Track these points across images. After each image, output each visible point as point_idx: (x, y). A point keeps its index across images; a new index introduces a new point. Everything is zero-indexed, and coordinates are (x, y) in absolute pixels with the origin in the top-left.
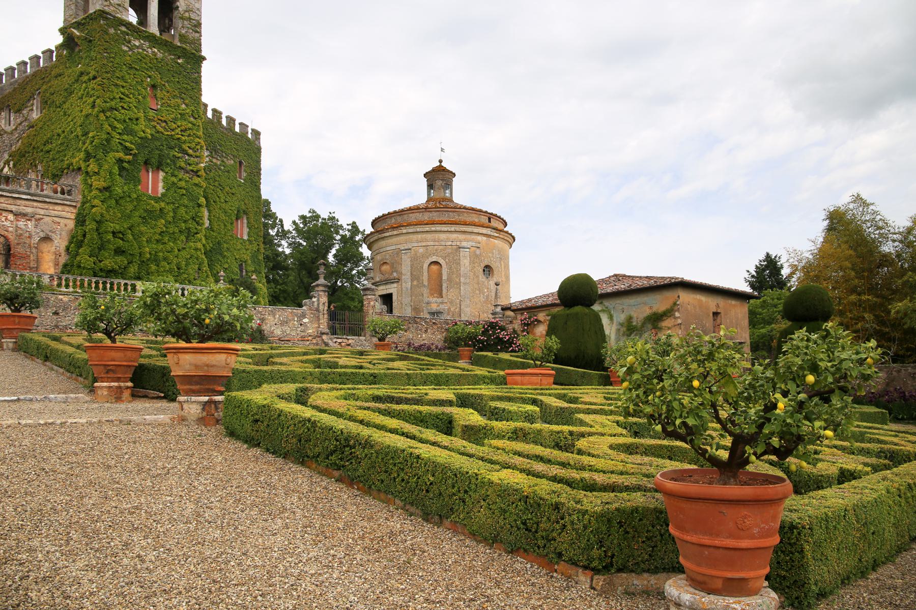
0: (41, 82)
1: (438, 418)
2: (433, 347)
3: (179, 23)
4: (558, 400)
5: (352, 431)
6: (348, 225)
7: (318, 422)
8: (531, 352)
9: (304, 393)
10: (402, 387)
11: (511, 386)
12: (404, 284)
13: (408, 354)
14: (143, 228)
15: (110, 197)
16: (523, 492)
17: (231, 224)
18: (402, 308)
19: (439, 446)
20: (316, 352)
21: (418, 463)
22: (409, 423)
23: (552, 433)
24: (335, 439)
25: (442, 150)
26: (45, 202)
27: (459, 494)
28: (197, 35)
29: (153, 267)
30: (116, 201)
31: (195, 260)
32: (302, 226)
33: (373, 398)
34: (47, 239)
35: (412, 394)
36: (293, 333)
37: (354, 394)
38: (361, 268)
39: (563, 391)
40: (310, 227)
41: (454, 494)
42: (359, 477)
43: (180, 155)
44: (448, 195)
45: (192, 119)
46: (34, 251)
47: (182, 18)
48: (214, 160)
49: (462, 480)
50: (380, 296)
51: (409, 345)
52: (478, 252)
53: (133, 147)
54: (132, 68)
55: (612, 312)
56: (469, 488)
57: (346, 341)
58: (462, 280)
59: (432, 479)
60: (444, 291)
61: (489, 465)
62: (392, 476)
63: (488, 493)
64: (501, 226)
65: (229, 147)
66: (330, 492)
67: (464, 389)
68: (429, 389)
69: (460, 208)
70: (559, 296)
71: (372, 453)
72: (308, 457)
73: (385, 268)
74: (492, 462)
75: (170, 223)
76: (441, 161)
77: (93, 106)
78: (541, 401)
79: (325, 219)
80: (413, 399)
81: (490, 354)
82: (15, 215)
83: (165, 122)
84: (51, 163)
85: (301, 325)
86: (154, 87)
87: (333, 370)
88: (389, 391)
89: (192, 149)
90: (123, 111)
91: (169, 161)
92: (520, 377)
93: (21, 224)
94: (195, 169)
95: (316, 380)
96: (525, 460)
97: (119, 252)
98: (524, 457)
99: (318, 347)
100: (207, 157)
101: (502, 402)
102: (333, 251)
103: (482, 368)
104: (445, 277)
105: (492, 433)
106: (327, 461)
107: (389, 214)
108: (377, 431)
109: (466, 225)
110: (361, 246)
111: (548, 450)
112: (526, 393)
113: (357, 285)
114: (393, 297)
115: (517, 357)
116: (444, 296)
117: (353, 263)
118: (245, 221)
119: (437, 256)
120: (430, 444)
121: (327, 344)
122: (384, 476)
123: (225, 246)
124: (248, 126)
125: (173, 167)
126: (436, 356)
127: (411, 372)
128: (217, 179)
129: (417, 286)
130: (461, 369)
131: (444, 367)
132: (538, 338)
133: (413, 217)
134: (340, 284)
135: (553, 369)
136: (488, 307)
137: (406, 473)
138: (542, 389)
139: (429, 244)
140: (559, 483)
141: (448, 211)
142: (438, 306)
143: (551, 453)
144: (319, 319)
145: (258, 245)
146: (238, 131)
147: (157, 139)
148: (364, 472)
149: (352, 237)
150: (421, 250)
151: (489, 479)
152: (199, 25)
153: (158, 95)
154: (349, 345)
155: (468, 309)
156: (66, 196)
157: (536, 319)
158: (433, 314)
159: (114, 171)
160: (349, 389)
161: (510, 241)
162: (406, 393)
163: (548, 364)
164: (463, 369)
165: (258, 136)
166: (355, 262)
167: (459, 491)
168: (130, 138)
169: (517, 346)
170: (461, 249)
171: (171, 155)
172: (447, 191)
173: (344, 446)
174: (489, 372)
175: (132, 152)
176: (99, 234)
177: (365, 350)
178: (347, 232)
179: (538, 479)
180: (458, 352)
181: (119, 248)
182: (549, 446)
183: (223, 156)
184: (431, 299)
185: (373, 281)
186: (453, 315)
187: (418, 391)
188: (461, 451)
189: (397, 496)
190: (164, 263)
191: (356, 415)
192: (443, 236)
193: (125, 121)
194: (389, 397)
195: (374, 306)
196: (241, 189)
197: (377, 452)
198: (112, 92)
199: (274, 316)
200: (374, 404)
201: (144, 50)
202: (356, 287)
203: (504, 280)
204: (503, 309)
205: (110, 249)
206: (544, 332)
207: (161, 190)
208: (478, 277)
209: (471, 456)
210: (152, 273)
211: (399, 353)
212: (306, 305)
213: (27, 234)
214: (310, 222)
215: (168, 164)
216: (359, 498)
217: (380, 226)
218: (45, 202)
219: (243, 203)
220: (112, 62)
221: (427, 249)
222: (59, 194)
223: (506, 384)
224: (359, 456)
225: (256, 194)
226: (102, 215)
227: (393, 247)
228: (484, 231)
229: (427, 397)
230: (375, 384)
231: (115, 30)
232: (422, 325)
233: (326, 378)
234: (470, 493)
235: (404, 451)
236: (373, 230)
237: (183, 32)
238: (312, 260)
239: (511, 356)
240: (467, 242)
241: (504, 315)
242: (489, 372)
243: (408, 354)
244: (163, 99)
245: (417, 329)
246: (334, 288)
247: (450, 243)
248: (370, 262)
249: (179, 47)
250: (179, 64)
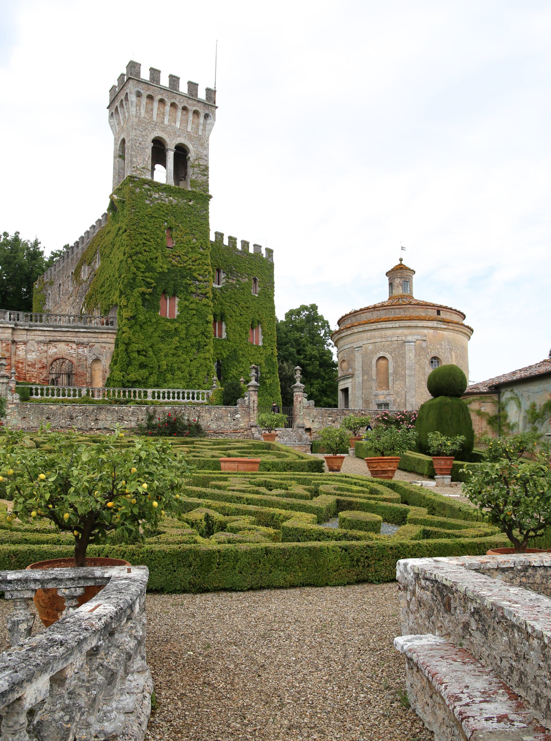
0: (100, 239)
3: (190, 171)
12: (357, 379)
14: (161, 346)
15: (135, 324)
17: (246, 333)
26: (95, 332)
28: (206, 177)
29: (169, 376)
30: (141, 326)
31: (205, 368)
34: (97, 360)
36: (227, 427)
43: (191, 282)
45: (201, 250)
46: (89, 370)
47: (193, 167)
48: (230, 281)
52: (424, 344)
53: (152, 281)
54: (152, 217)
55: (520, 399)
58: (407, 372)
60: (391, 384)
65: (243, 267)
75: (183, 339)
76: (401, 260)
77: (125, 254)
82: (77, 344)
83: (179, 256)
84: (104, 302)
85: (234, 420)
86: (170, 229)
89: (202, 275)
90: (145, 254)
91: (182, 288)
93: (80, 351)
94: (204, 292)
97: (142, 366)
100: (223, 279)
104: (391, 371)
116: (390, 388)
118: (260, 330)
119: (384, 351)
123: (241, 352)
124: (261, 247)
125: (185, 293)
128: (233, 296)
133: (364, 317)
139: (377, 340)
141: (394, 309)
142: (385, 397)
144: (249, 414)
145: (272, 349)
146: (253, 252)
147: (173, 272)
150: (371, 347)
152: (207, 168)
153: (174, 236)
155: (413, 399)
156: (110, 326)
158: (379, 405)
159: (139, 303)
165: (270, 254)
168: (151, 274)
170: (406, 344)
171: (184, 283)
175: (153, 285)
176: (128, 353)
181: (142, 363)
183: (238, 276)
186: (399, 405)
190: (178, 373)
192: (389, 332)
193: (147, 261)
196: (255, 303)
198: (137, 239)
199: (210, 414)
201: (163, 200)
205: (136, 365)
207: (177, 313)
208: (424, 368)
210: (168, 380)
213: (84, 358)
215: (181, 291)
218: (95, 332)
219: (257, 314)
220: (137, 215)
221: (375, 346)
222: (105, 325)
225: (270, 305)
226: (129, 339)
227: (349, 346)
228: (430, 324)
231: (140, 189)
237: (194, 178)
240: (412, 336)
244: (177, 237)
247: (396, 338)
249: (190, 191)
250: (190, 206)
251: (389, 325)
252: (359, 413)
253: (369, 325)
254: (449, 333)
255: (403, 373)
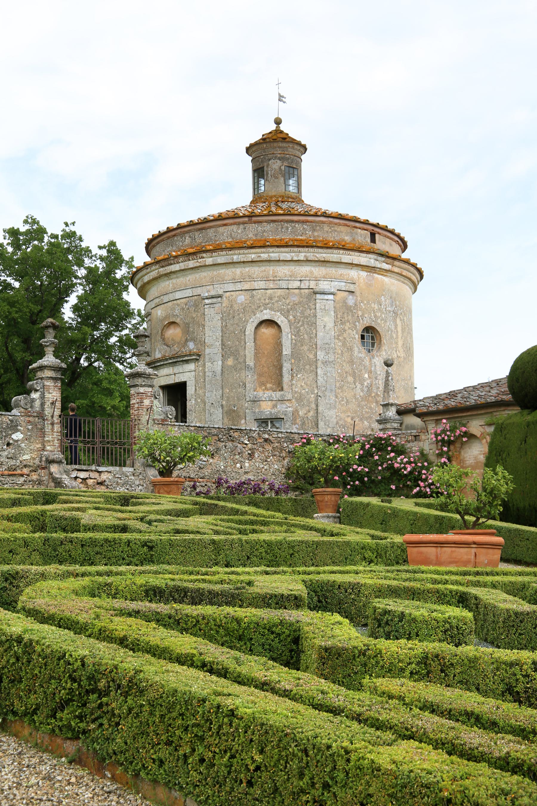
1: (273, 633)
2: (265, 487)
4: (511, 598)
5: (104, 662)
6: (100, 248)
7: (38, 642)
8: (456, 498)
9: (11, 583)
10: (204, 570)
11: (415, 567)
12: (208, 364)
13: (216, 502)
16: (441, 791)
18: (204, 410)
19: (274, 691)
20: (37, 499)
21: (231, 725)
22: (216, 642)
23: (499, 664)
24: (70, 676)
25: (281, 98)
27: (313, 791)
32: (10, 249)
33: (147, 592)
35: (222, 582)
37: (109, 585)
38: (126, 332)
39: (520, 579)
40: (26, 253)
41: (302, 791)
42: (115, 753)
44: (292, 189)
49: (318, 761)
50: (163, 387)
51: (219, 483)
52: (351, 300)
56: (332, 778)
57: (96, 475)
58: (321, 355)
59: (258, 758)
60: (286, 378)
61: (372, 730)
62: (181, 752)
63: (371, 790)
64: (394, 250)
66: (57, 785)
67: (324, 572)
68: (256, 572)
69: (316, 215)
70: (509, 387)
71: (142, 706)
72: (15, 713)
73: (171, 332)
74: (378, 725)
76: (278, 122)
78: (476, 598)
79: (56, 237)
80: (222, 594)
81: (374, 501)
85: (8, 444)
87: (70, 535)
88: (177, 577)
92: (434, 549)
95: (36, 556)
96: (444, 721)
98: (442, 714)
99: (41, 489)
101: (399, 601)
102: (73, 299)
103: (359, 530)
104: (286, 351)
105: (378, 663)
106: (53, 721)
107: (180, 227)
108: (153, 660)
109: (327, 248)
110: (126, 288)
111: (492, 702)
112: (446, 582)
113: (117, 364)
114: (188, 388)
115: (429, 506)
116: (285, 387)
117: (111, 323)
119: (271, 309)
120: (256, 687)
121: (58, 483)
122: (164, 753)
126: (270, 505)
127: (222, 537)
129: (234, 367)
130: (317, 530)
131: (285, 527)
132: (469, 470)
134: (86, 364)
135: (499, 532)
136: (370, 408)
137: (208, 747)
138: (477, 574)
139: (256, 285)
140: (514, 772)
141: (292, 221)
142: (275, 406)
143: (498, 708)
144: (43, 434)
148: (126, 743)
149: (109, 272)
150: (242, 298)
151: (373, 761)
154: (101, 483)
155: (332, 413)
157: (465, 433)
158: (263, 422)
160: (99, 574)
161: (413, 278)
162: (210, 582)
163: (491, 522)
164: (323, 532)
166: (114, 320)
167: (313, 785)
169: (429, 485)
170: (318, 296)
172: (291, 182)
173: (88, 692)
174: (373, 537)
177: (133, 493)
178: (98, 262)
179: (471, 763)
180: (313, 496)
182: (493, 691)
184: (260, 393)
185: (149, 359)
186: (303, 423)
187: (233, 577)
188: (316, 701)
189: (190, 793)
191: (111, 626)
192: (283, 270)
194: (177, 589)
195: (150, 409)
197: (151, 705)
200: (148, 604)
202: (117, 369)
203: (402, 355)
204: (400, 413)
206: (482, 458)
208: (351, 349)
209: (335, 711)
211: (198, 499)
212: (17, 406)
214: (27, 242)
216: (115, 798)
217: (161, 252)
221: (253, 296)
223: (406, 561)
224: (117, 712)
227: (189, 293)
229: (251, 590)
230: (151, 561)
232: (243, 443)
233: (55, 550)
234: (335, 789)
235: (204, 701)
236: (148, 259)
238: (31, 317)
239: (417, 504)
241: (401, 424)
242: (373, 537)
243: (216, 502)
245: (233, 451)
246: (74, 373)
247: (297, 284)
248: (143, 321)
251: (286, 254)
252: (260, 436)
253: (242, 251)
254: (393, 281)
255: (311, 356)
